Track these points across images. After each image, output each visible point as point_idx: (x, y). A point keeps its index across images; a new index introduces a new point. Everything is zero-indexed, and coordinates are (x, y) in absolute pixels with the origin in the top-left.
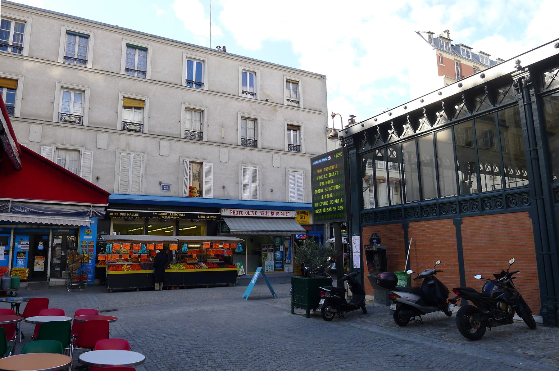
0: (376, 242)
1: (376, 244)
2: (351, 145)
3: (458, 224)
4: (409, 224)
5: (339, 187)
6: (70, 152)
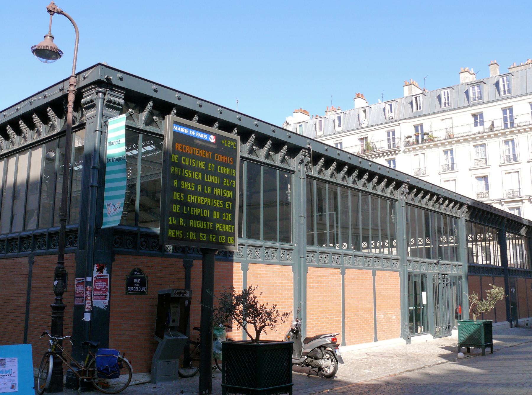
0: (138, 283)
1: (138, 287)
2: (189, 160)
3: (343, 273)
4: (193, 261)
5: (178, 209)
6: (12, 194)
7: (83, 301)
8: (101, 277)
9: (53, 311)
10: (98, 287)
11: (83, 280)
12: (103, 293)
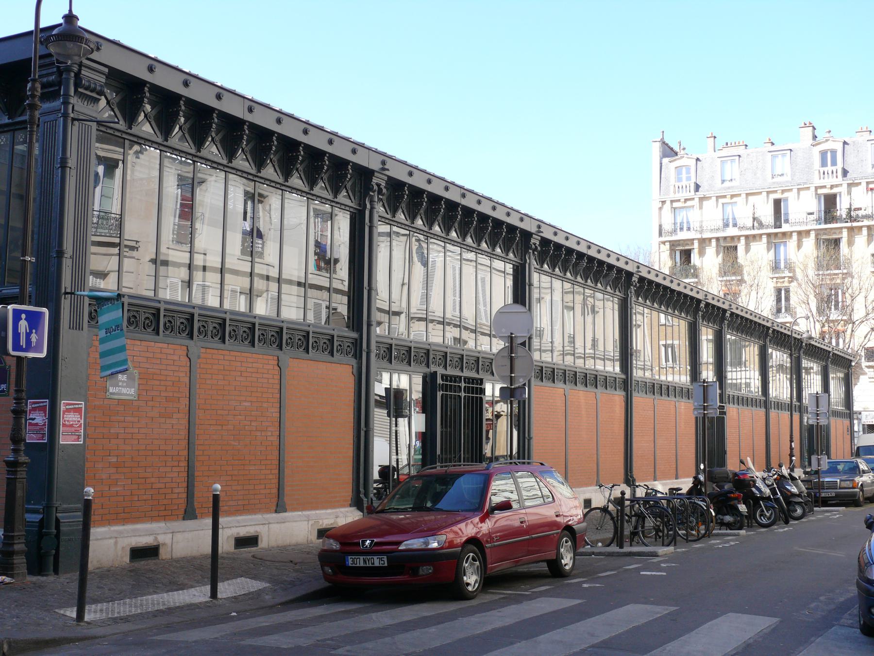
7: (43, 437)
8: (73, 407)
9: (8, 469)
10: (68, 421)
11: (44, 404)
12: (75, 431)
